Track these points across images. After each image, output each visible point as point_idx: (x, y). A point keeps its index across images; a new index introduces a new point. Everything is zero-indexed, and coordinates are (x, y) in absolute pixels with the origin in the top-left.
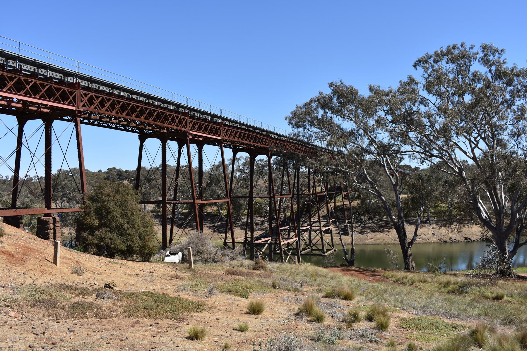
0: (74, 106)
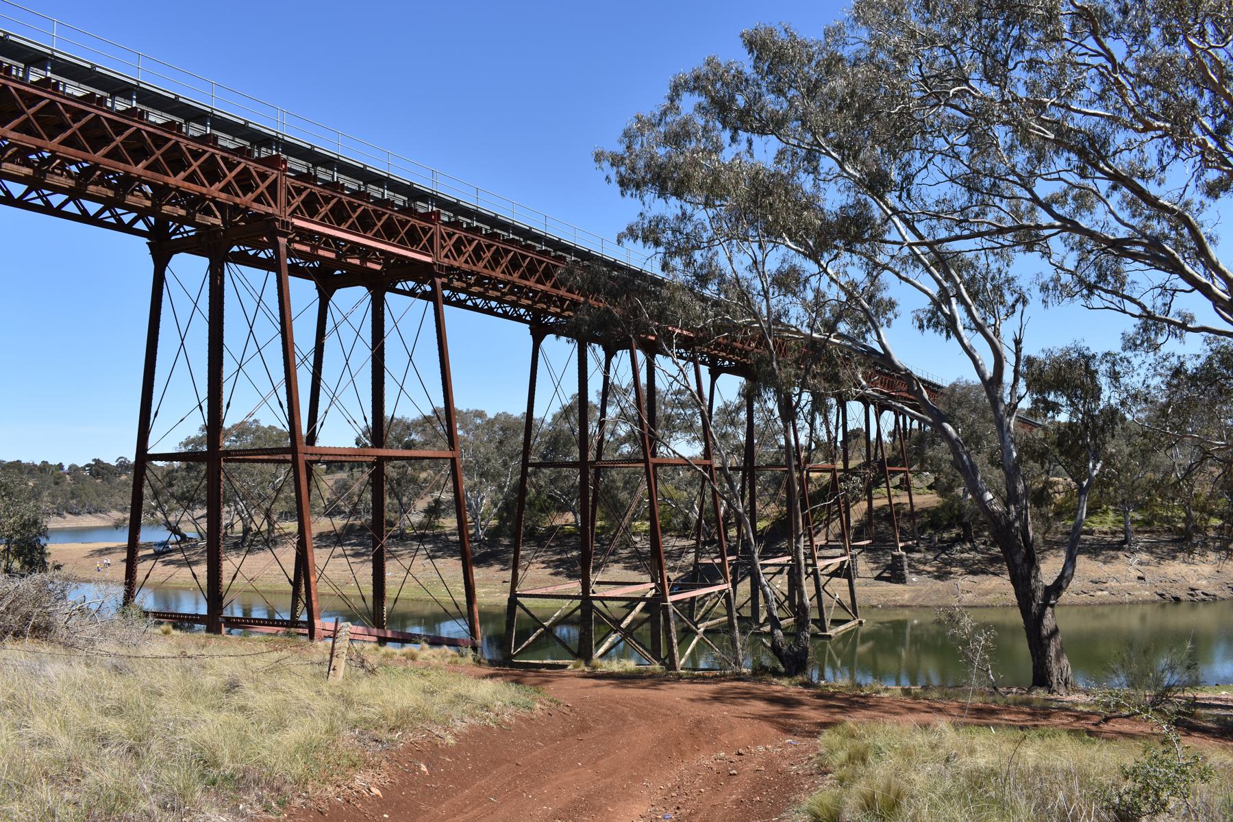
0: (430, 256)
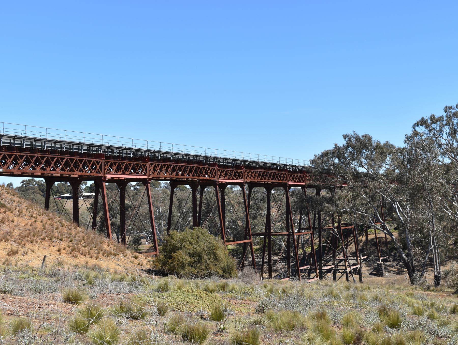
0: (146, 176)
